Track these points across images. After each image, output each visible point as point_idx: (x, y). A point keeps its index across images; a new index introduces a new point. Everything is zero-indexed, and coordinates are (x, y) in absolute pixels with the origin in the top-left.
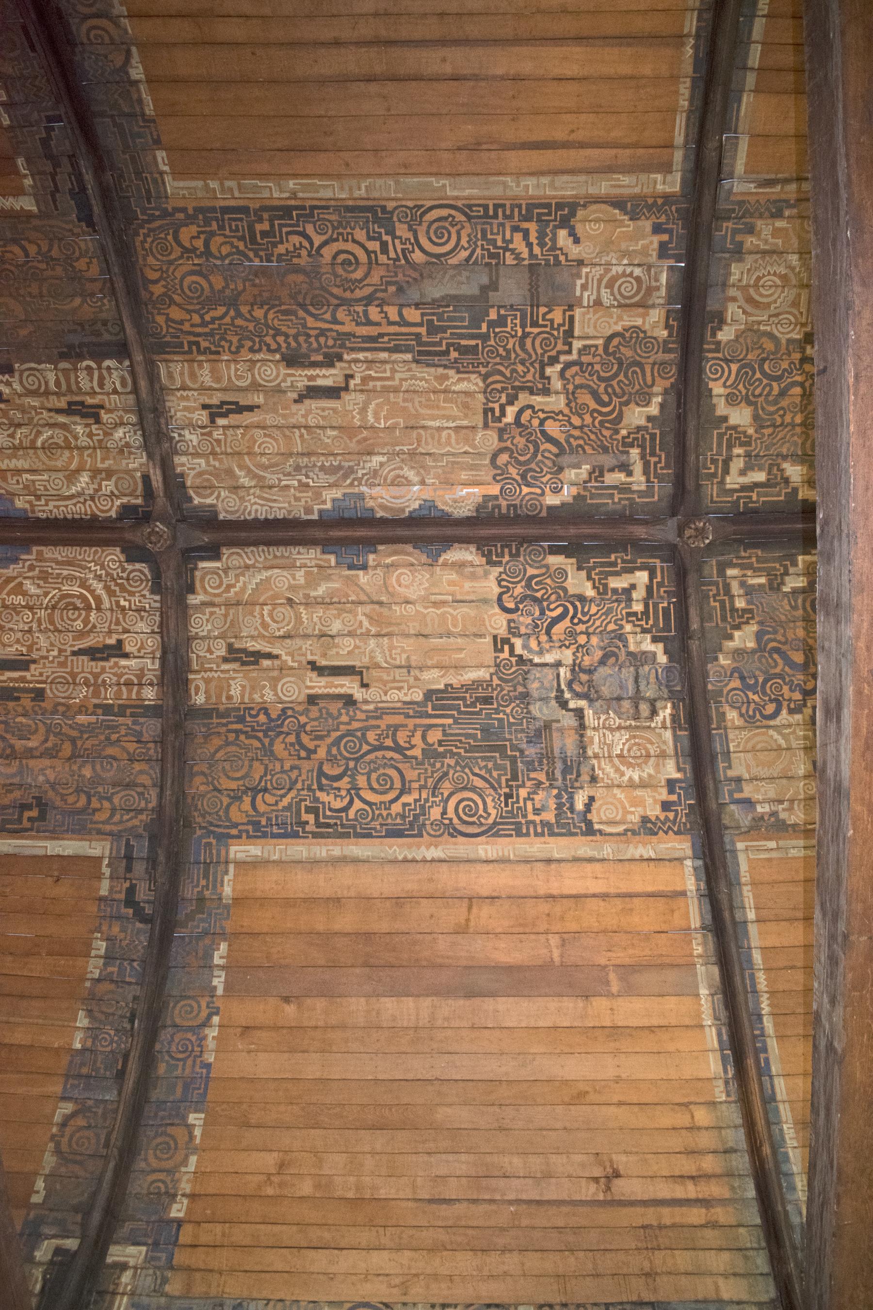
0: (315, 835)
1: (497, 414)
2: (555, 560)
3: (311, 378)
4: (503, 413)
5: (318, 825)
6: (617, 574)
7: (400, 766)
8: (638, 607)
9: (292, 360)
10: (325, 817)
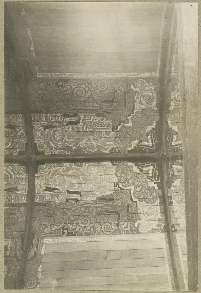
0: (67, 236)
1: (116, 128)
2: (130, 164)
3: (70, 120)
4: (117, 128)
5: (68, 233)
6: (145, 167)
7: (90, 217)
8: (151, 175)
9: (66, 115)
10: (70, 231)
